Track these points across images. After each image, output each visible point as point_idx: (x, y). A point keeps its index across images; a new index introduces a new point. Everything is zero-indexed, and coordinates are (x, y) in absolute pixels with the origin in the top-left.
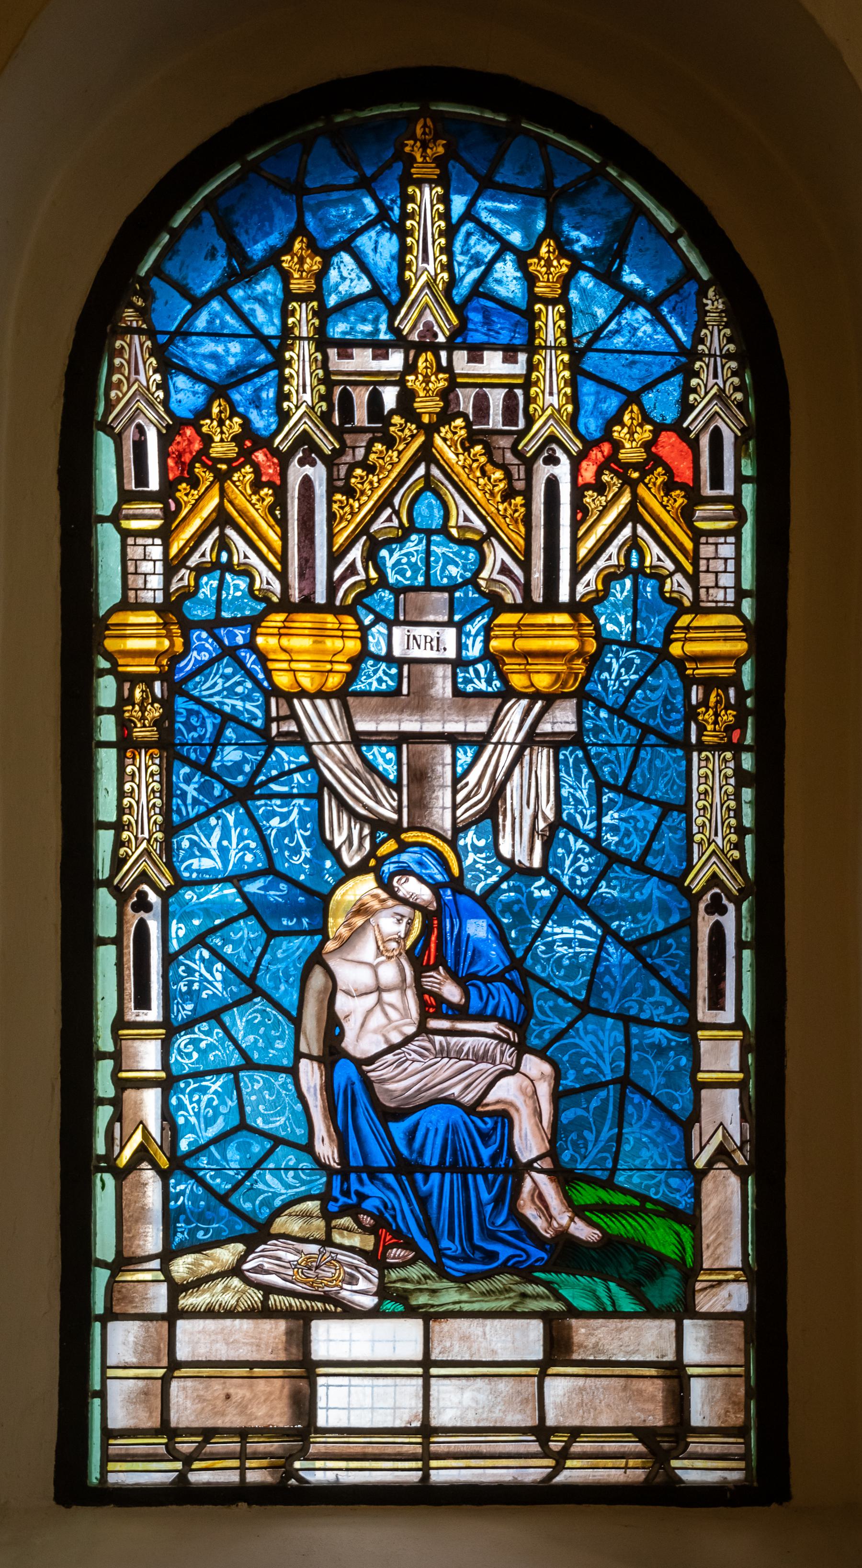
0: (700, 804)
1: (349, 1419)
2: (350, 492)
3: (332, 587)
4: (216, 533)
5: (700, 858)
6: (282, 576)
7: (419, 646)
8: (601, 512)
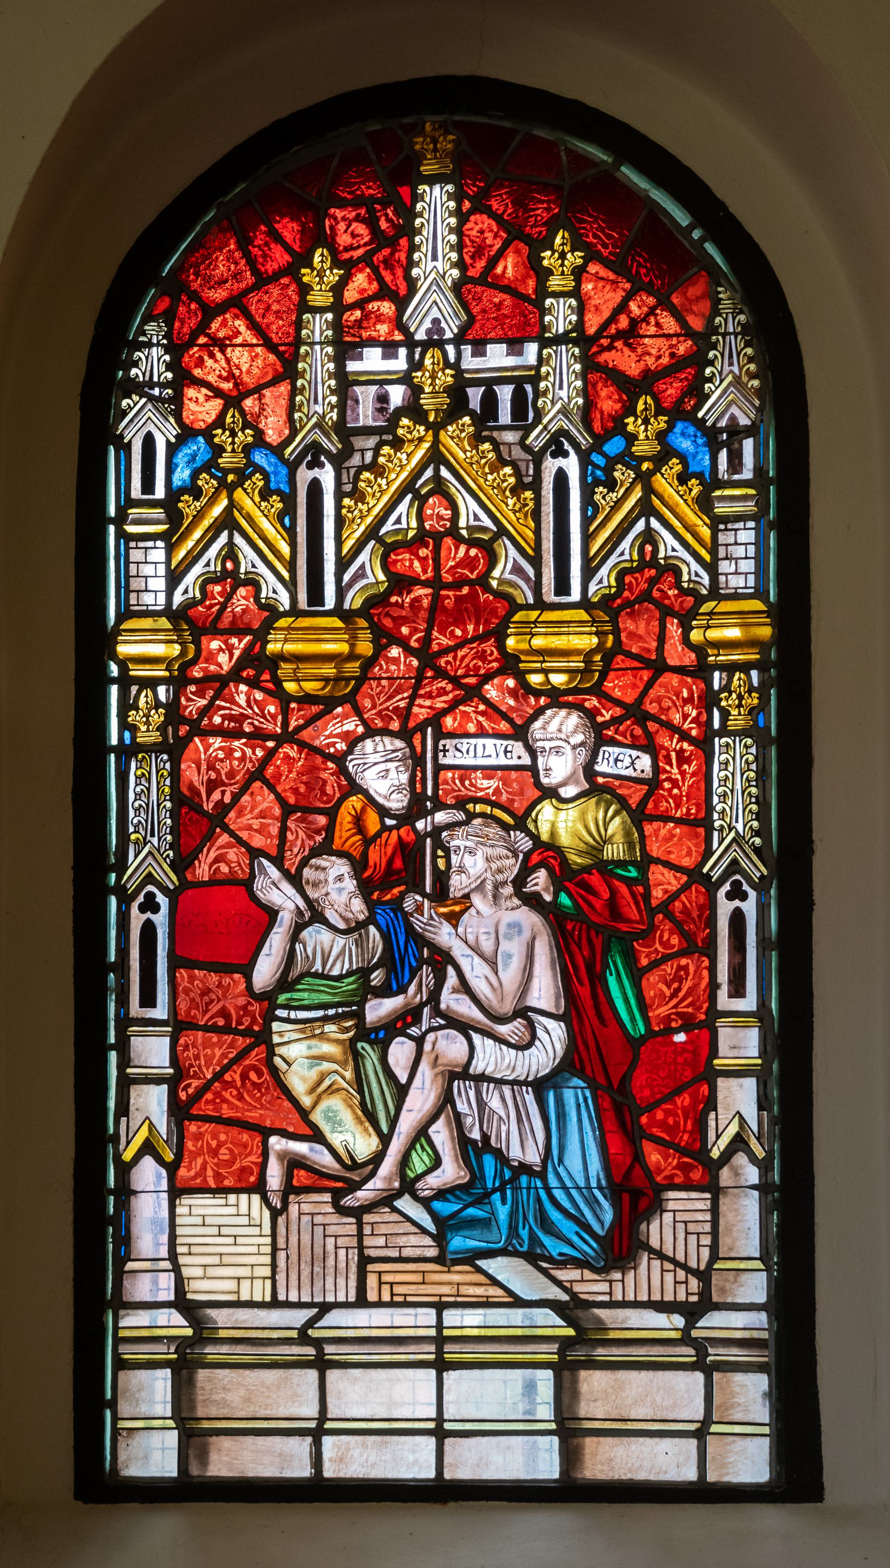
0: (722, 774)
1: (428, 1404)
4: (223, 538)
5: (720, 844)
6: (291, 586)
8: (612, 508)
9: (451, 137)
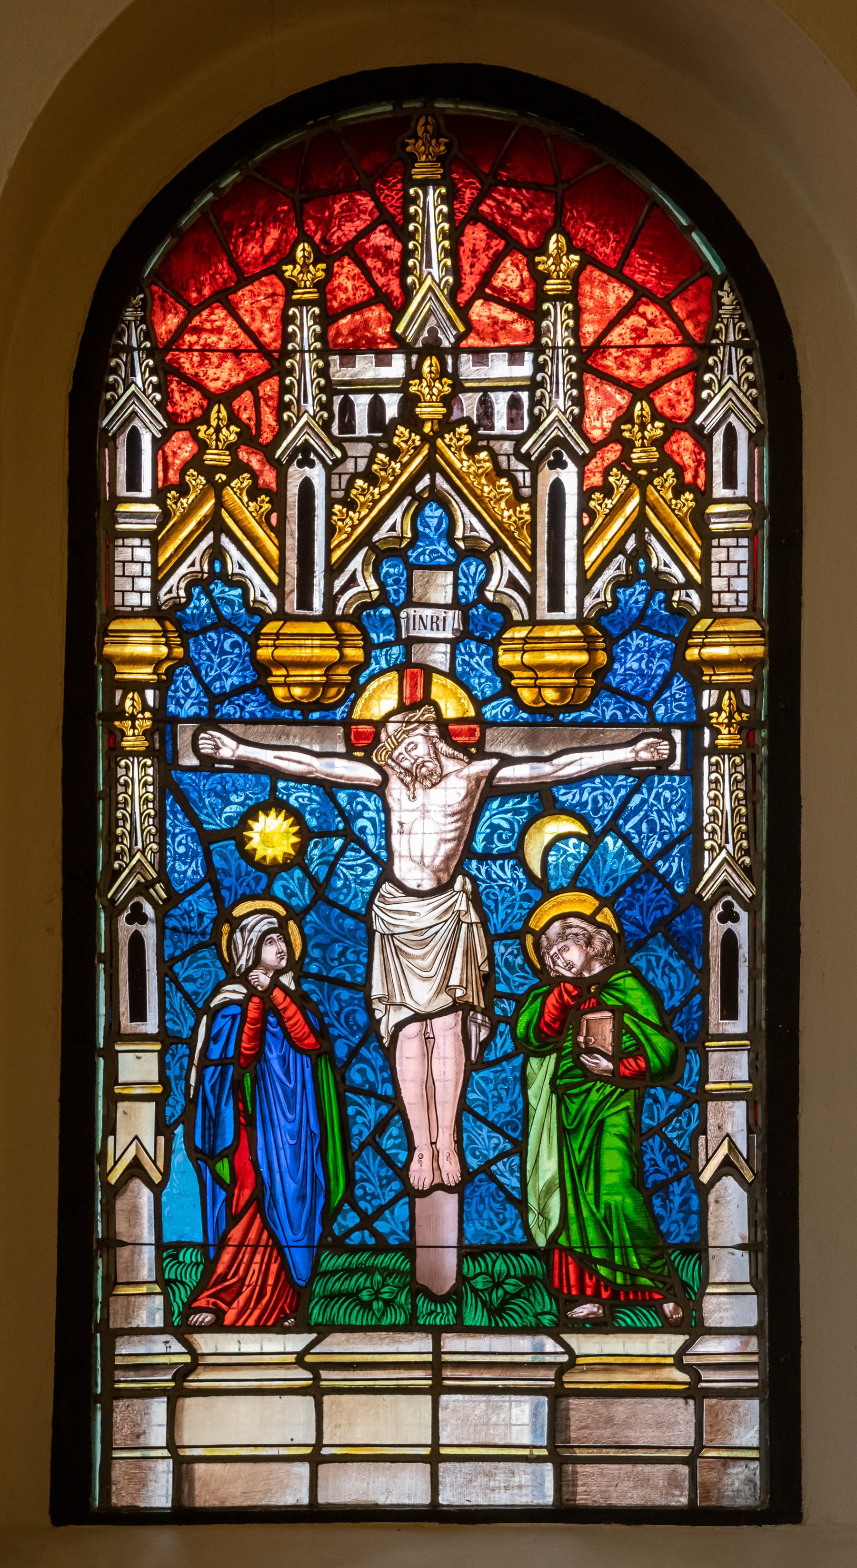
0: (713, 776)
2: (351, 505)
3: (331, 599)
4: (209, 539)
5: (710, 865)
6: (279, 591)
7: (425, 628)
9: (443, 140)
